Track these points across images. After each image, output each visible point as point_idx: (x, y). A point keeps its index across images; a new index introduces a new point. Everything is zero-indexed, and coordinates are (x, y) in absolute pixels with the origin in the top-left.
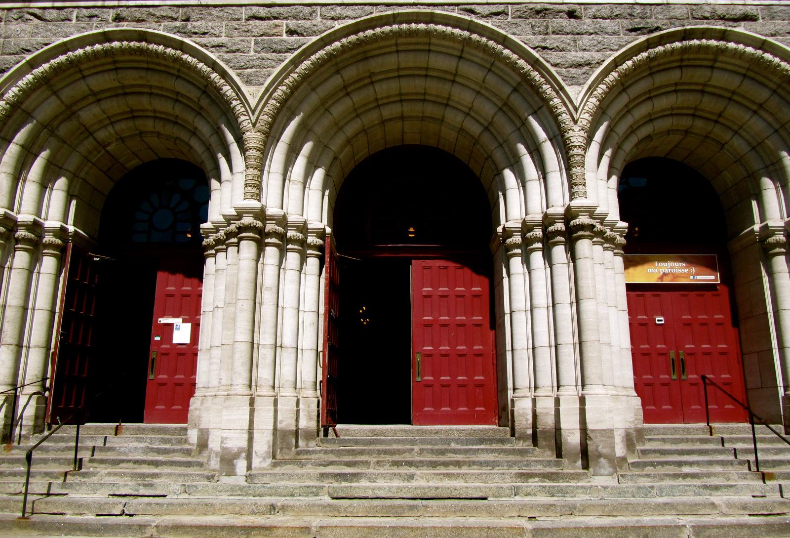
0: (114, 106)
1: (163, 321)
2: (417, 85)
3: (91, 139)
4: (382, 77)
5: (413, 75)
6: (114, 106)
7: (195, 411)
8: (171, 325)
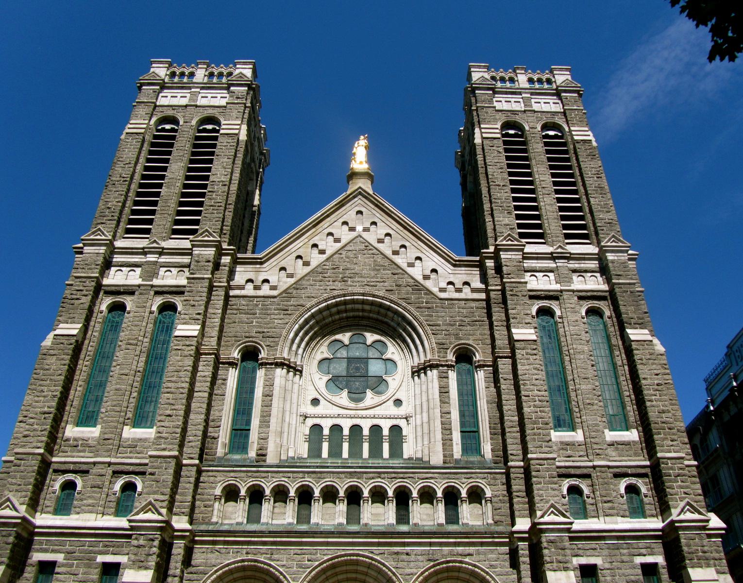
2: (354, 575)
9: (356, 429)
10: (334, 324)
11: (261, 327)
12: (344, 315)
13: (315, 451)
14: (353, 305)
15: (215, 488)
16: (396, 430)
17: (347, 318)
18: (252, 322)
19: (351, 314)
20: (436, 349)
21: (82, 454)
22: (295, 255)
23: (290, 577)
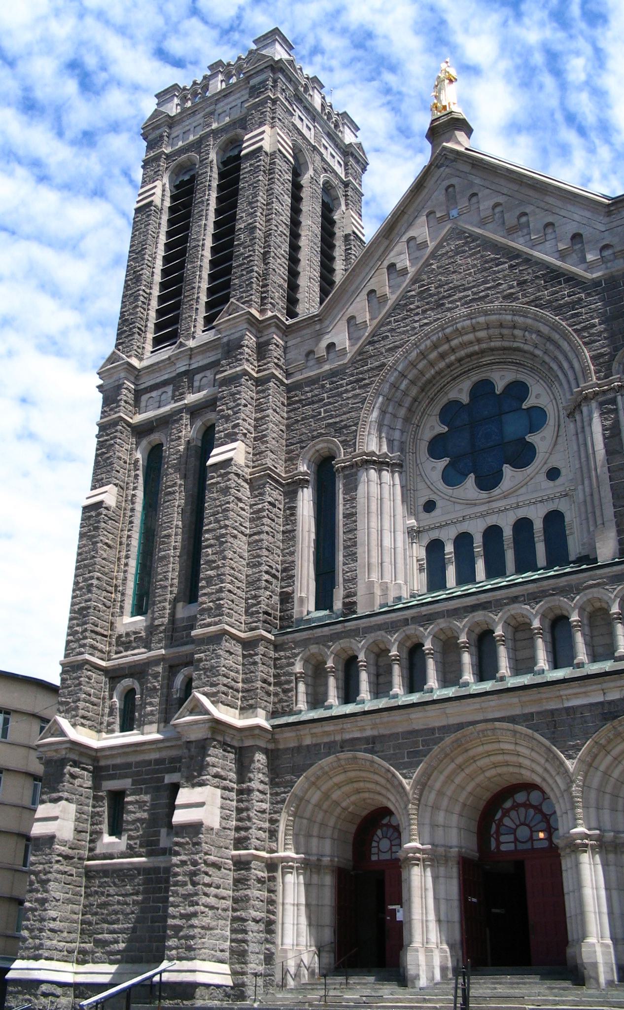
0: (347, 789)
1: (391, 907)
2: (500, 758)
3: (339, 808)
4: (480, 757)
5: (496, 754)
6: (347, 789)
7: (573, 419)
8: (395, 910)
9: (493, 534)
10: (442, 377)
11: (332, 417)
12: (453, 358)
13: (436, 581)
14: (460, 339)
15: (293, 664)
16: (554, 519)
17: (459, 360)
18: (320, 413)
19: (462, 353)
20: (592, 367)
21: (136, 651)
22: (365, 292)
23: (400, 774)
